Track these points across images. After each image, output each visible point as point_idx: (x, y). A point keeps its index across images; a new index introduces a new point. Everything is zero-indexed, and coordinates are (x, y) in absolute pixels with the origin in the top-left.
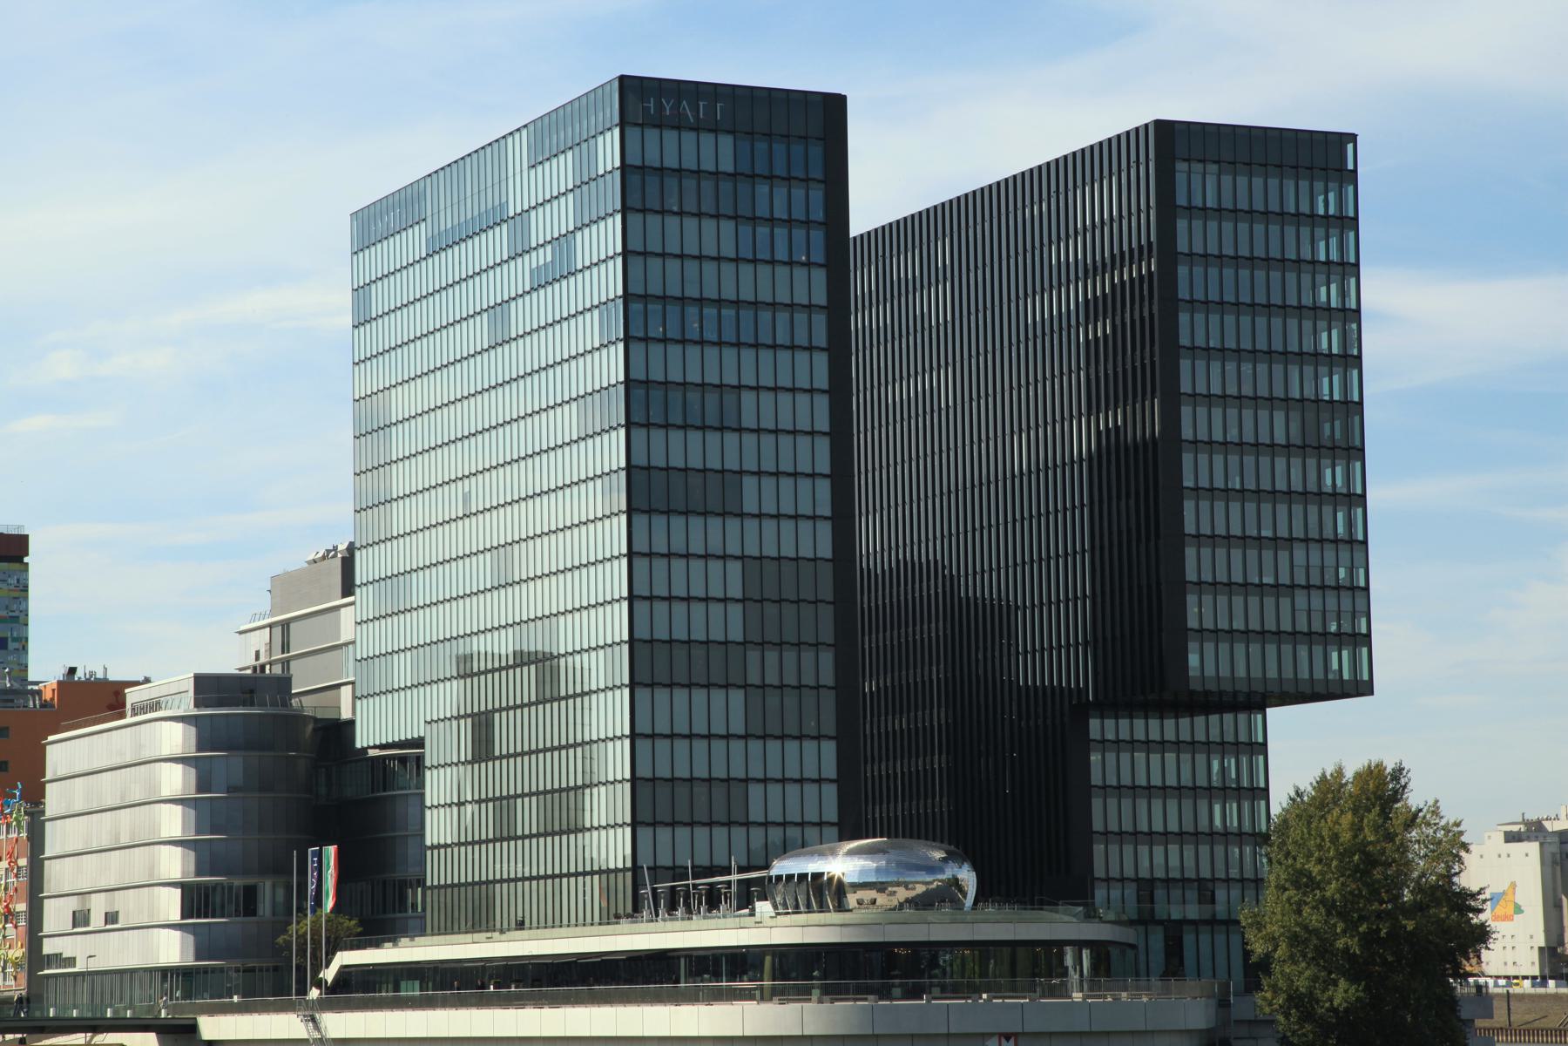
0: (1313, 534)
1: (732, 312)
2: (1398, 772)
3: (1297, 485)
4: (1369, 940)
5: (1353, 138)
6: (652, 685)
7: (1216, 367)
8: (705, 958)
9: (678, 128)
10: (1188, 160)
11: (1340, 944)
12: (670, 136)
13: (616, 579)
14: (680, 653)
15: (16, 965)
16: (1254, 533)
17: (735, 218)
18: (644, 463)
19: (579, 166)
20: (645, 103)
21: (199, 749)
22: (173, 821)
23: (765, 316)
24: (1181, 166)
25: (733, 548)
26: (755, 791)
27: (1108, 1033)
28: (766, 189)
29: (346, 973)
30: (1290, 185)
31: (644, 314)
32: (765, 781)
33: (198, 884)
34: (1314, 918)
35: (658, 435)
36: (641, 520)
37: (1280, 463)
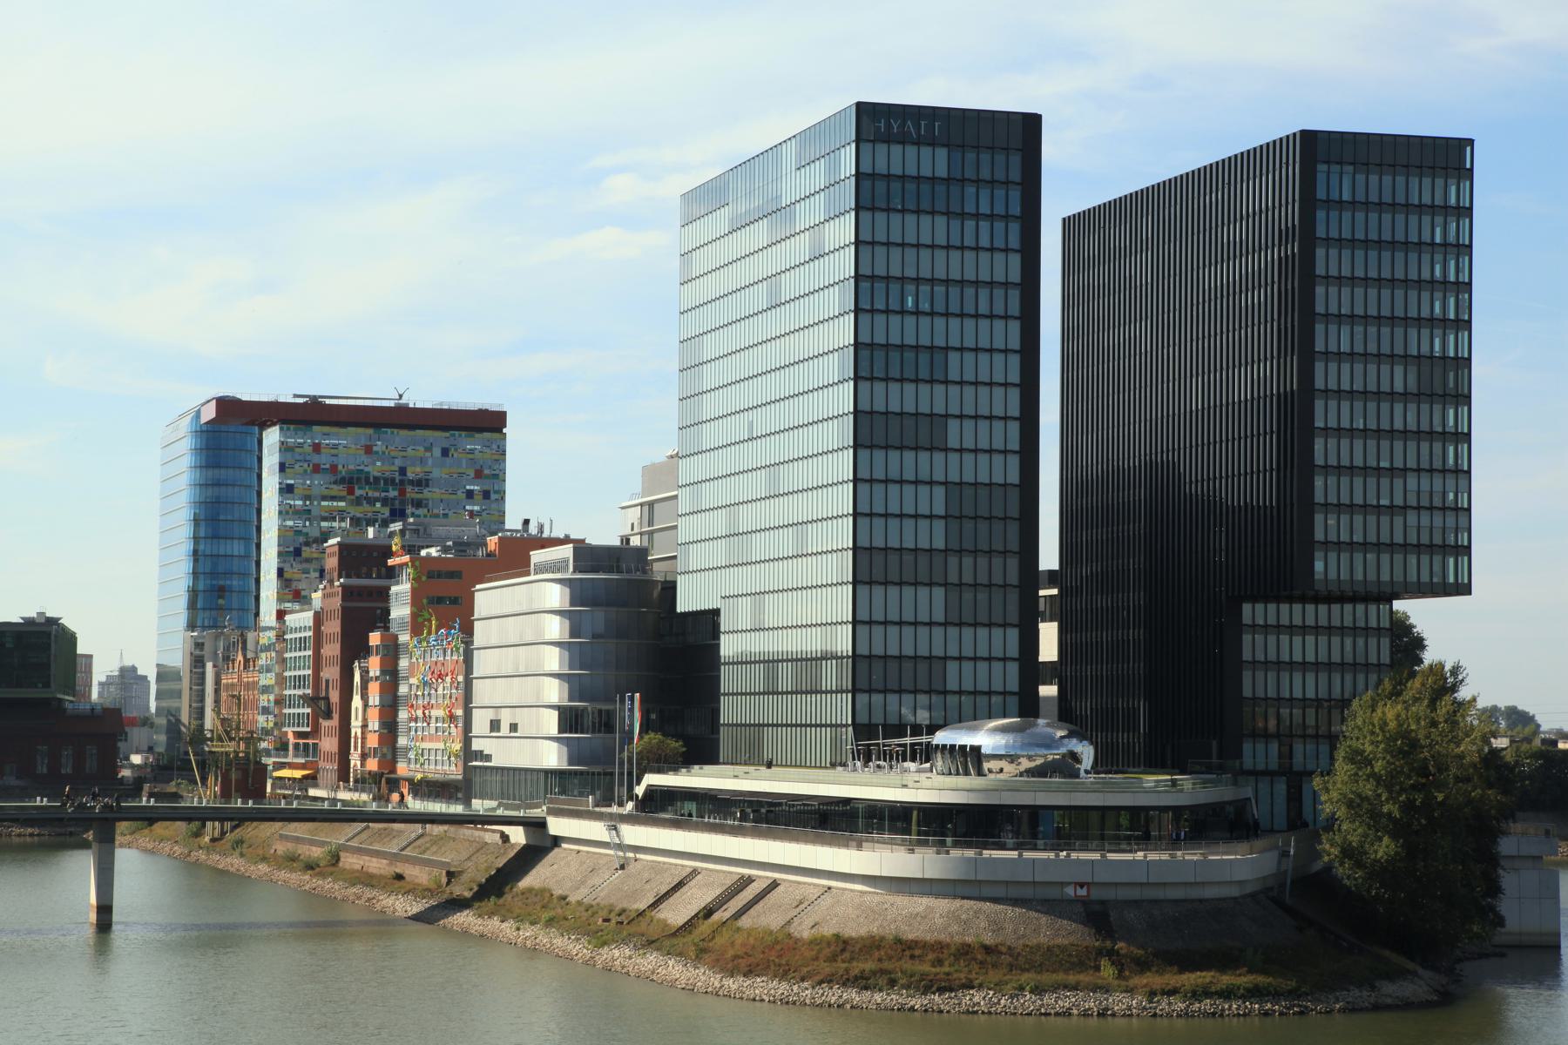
0: (1425, 465)
1: (943, 289)
2: (1455, 671)
3: (1412, 426)
4: (1408, 807)
5: (1471, 142)
6: (870, 583)
7: (1345, 330)
8: (882, 810)
9: (903, 143)
10: (1328, 162)
11: (1385, 809)
12: (896, 149)
13: (843, 500)
14: (893, 559)
15: (457, 756)
16: (1374, 464)
17: (947, 213)
18: (868, 409)
19: (828, 171)
20: (878, 124)
21: (572, 604)
22: (553, 660)
23: (969, 292)
24: (1322, 168)
25: (939, 476)
26: (952, 667)
27: (1165, 884)
28: (973, 190)
29: (652, 792)
30: (1414, 181)
31: (872, 292)
32: (960, 659)
33: (571, 708)
34: (1368, 789)
35: (879, 387)
36: (864, 454)
37: (1398, 408)
